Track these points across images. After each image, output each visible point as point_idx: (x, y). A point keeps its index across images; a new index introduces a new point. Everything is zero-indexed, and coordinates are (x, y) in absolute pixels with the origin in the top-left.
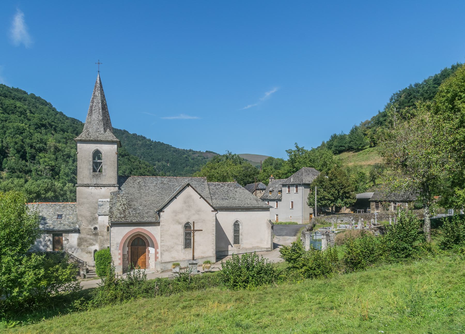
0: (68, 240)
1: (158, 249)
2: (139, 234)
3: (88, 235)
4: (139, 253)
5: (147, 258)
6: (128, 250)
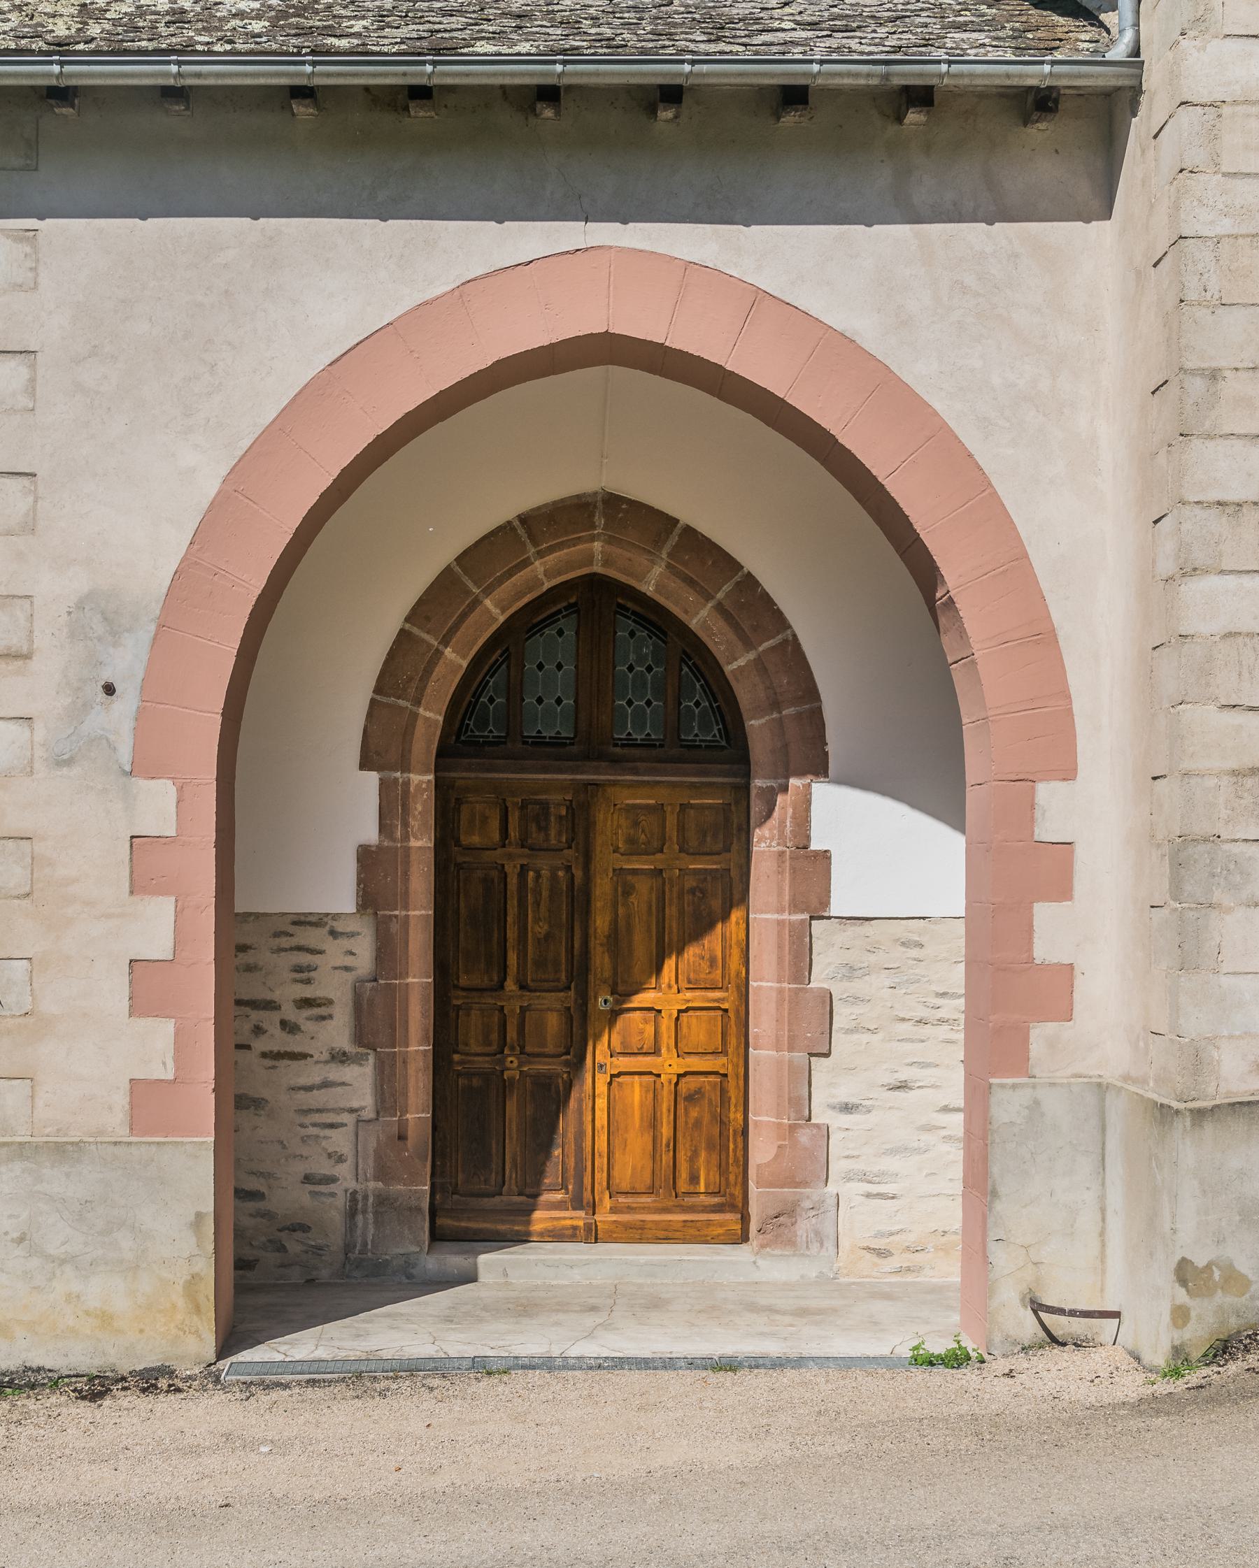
1: (1068, 773)
2: (613, 502)
4: (601, 922)
5: (763, 1024)
6: (370, 833)
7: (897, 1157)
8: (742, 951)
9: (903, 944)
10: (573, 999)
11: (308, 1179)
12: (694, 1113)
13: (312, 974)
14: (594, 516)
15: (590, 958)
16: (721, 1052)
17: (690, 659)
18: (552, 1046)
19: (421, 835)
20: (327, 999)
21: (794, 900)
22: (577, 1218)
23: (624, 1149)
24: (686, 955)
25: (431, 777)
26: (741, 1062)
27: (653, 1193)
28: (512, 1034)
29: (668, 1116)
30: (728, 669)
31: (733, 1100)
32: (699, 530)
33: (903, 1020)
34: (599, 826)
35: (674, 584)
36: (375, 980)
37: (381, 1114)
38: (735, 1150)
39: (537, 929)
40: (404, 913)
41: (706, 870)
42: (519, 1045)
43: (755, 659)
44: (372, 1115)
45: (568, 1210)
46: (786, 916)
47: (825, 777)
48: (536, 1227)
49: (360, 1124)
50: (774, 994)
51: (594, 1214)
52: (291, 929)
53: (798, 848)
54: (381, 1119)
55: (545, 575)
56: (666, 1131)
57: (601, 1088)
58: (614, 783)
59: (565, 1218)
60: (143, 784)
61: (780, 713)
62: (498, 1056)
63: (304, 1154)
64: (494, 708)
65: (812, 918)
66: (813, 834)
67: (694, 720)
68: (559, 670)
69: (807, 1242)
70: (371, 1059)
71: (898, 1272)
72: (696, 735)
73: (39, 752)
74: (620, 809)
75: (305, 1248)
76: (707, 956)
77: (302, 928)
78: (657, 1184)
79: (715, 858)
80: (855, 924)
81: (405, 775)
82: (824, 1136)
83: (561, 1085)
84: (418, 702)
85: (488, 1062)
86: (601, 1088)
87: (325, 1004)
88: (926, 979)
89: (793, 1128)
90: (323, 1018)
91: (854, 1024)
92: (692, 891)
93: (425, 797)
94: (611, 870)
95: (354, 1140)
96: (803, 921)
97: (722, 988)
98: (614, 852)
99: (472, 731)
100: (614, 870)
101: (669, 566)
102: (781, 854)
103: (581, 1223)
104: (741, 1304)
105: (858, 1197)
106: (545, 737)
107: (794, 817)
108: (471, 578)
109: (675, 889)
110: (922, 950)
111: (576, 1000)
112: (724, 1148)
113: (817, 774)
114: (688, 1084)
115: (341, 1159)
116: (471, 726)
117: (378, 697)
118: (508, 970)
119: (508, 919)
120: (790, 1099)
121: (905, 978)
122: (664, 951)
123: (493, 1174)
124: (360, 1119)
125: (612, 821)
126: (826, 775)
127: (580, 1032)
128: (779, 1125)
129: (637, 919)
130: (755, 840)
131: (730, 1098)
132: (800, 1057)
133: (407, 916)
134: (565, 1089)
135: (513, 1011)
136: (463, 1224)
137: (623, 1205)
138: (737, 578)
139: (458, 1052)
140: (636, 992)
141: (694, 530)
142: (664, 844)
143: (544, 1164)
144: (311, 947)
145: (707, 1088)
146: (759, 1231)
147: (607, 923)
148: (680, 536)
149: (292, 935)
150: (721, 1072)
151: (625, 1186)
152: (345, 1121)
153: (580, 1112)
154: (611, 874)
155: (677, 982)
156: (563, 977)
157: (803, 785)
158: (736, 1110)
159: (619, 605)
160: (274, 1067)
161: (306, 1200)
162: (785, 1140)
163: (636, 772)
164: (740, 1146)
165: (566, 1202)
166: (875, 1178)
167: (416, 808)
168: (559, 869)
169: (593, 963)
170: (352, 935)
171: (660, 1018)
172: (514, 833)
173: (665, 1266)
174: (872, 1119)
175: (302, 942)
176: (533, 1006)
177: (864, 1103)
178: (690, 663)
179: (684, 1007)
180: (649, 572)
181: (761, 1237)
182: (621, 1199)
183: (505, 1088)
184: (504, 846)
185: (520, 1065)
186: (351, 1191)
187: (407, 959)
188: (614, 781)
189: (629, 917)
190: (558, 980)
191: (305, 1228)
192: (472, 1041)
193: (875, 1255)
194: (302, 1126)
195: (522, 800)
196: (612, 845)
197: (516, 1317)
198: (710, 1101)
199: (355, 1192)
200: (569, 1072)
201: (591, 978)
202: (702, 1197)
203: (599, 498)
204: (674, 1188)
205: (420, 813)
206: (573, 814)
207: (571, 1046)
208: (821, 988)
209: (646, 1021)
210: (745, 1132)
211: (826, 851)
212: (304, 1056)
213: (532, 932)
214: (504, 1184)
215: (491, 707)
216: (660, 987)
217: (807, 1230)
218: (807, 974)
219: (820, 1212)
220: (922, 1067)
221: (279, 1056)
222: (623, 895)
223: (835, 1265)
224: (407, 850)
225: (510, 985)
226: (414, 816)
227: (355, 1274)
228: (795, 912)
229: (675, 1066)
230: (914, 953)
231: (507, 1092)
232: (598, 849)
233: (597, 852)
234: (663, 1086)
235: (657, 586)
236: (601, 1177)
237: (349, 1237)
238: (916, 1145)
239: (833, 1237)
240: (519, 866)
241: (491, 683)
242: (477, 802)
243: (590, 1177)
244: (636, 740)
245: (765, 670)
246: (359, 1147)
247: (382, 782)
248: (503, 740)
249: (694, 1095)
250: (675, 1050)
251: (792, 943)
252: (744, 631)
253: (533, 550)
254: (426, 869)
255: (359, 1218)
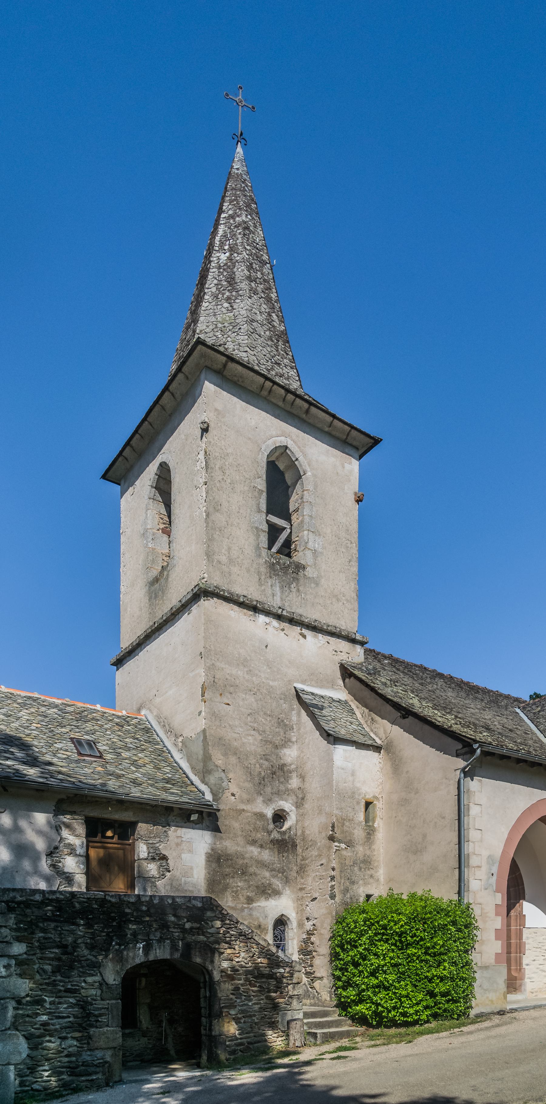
0: (164, 858)
3: (254, 842)
60: (497, 894)
73: (483, 887)
230: (536, 934)
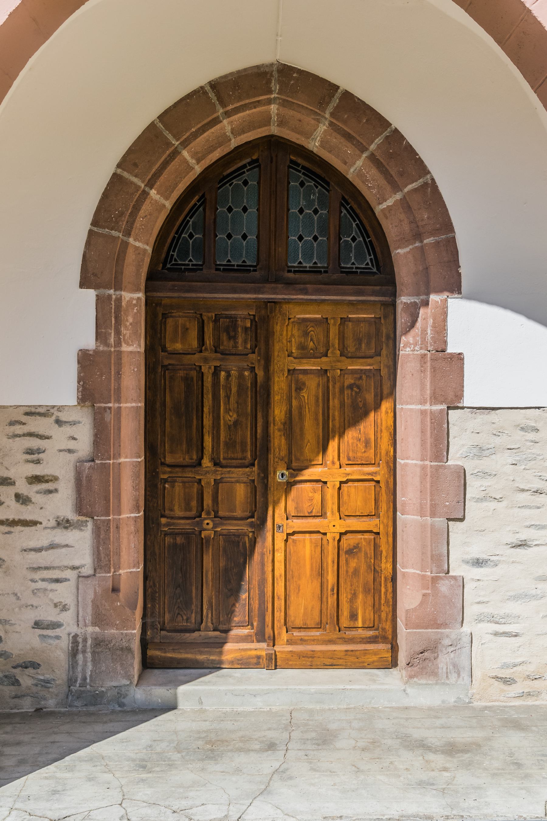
7: (519, 602)
8: (390, 434)
9: (522, 429)
10: (256, 472)
11: (37, 625)
12: (353, 564)
13: (41, 456)
14: (271, 83)
15: (270, 441)
16: (374, 515)
17: (348, 204)
18: (240, 512)
19: (132, 341)
20: (53, 476)
21: (434, 393)
22: (260, 649)
23: (298, 593)
24: (346, 437)
25: (141, 295)
26: (391, 523)
27: (321, 628)
28: (208, 501)
29: (333, 567)
30: (378, 209)
31: (384, 553)
32: (355, 95)
33: (523, 490)
34: (277, 334)
35: (336, 140)
36: (93, 460)
37: (98, 571)
38: (386, 593)
39: (228, 417)
40: (117, 405)
41: (362, 370)
42: (213, 511)
43: (401, 199)
44: (91, 572)
45: (253, 642)
46: (427, 407)
47: (458, 293)
48: (227, 657)
49: (80, 579)
50: (418, 470)
51: (274, 646)
52: (24, 419)
53: (437, 351)
54: (98, 575)
55: (232, 133)
56: (331, 578)
57: (280, 544)
58: (288, 302)
59: (251, 650)
61: (421, 242)
62: (197, 519)
63: (35, 604)
64: (192, 242)
65: (449, 408)
66: (449, 340)
67: (351, 251)
68: (245, 213)
69: (447, 673)
70: (90, 525)
71: (521, 696)
72: (353, 264)
74: (294, 322)
75: (35, 682)
76: (363, 439)
77: (33, 417)
78: (324, 621)
79: (369, 361)
80: (484, 413)
81: (118, 293)
82: (460, 586)
83: (247, 542)
84: (128, 233)
85: (188, 524)
86: (280, 544)
87: (51, 481)
88: (541, 457)
89: (435, 580)
90: (50, 492)
91: (483, 494)
92: (351, 387)
93: (135, 311)
94: (286, 370)
95: (76, 593)
96: (441, 411)
97: (374, 464)
98: (289, 356)
99: (176, 260)
100: (289, 371)
101: (331, 124)
102: (424, 356)
103: (263, 653)
104: (397, 738)
105: (487, 635)
106: (234, 265)
107: (434, 326)
108: (171, 132)
109: (338, 385)
110: (538, 434)
111: (259, 474)
112: (377, 591)
113: (452, 291)
114: (349, 541)
115: (65, 608)
116: (175, 256)
117: (95, 229)
118: (205, 450)
119: (205, 409)
120: (432, 556)
121: (525, 456)
122: (329, 435)
123: (193, 615)
124: (81, 575)
125: (287, 331)
126: (460, 292)
127: (262, 499)
128: (423, 577)
129: (307, 410)
130: (402, 345)
131: (382, 552)
132: (440, 521)
133: (120, 408)
134: (250, 545)
135: (208, 483)
136: (169, 655)
137: (297, 638)
138: (386, 133)
139: (163, 516)
140: (306, 468)
141: (352, 94)
142: (328, 350)
143: (234, 605)
144: (40, 433)
145: (364, 543)
146: (408, 664)
147: (283, 413)
148: (341, 99)
149: (24, 424)
150: (375, 531)
151: (299, 622)
152: (68, 577)
153: (263, 564)
154: (286, 374)
155: (339, 459)
156: (249, 455)
157: (441, 300)
158: (387, 562)
159: (292, 161)
160: (9, 533)
161: (36, 642)
162: (428, 589)
163: (305, 292)
164: (390, 590)
165: (251, 636)
166: (501, 620)
167: (127, 320)
168: (244, 369)
169: (272, 445)
170: (74, 423)
171: (326, 487)
172: (209, 341)
173: (332, 694)
174: (498, 571)
175: (33, 429)
176: (225, 479)
177: (492, 558)
178: (348, 207)
179: (344, 479)
180: (315, 130)
181: (409, 669)
182: (296, 633)
183: (203, 544)
184: (201, 351)
185: (215, 526)
186: (73, 634)
187: (120, 442)
188: (288, 299)
189: (300, 408)
190: (244, 458)
191: (35, 665)
192: (176, 508)
193: (502, 683)
194: (33, 581)
195: (216, 315)
196: (287, 350)
197: (202, 760)
198: (366, 554)
199: (76, 636)
200: (253, 532)
201: (271, 456)
202: (360, 631)
203: (275, 68)
204: (338, 624)
205: (131, 324)
206: (256, 326)
207: (255, 511)
208: (457, 465)
209: (314, 491)
210: (394, 579)
211: (460, 354)
212: (34, 523)
213: (224, 420)
214: (202, 622)
215: (191, 242)
216: (326, 463)
217: (447, 663)
218: (445, 453)
219: (457, 648)
220: (539, 529)
221: (13, 523)
222: (296, 390)
223: (470, 692)
224: (119, 354)
225: (206, 462)
226: (126, 327)
227: (76, 703)
228: (435, 404)
229: (337, 526)
230: (531, 436)
231: (204, 549)
232: (276, 354)
233: (276, 357)
234: (328, 543)
235: (322, 141)
236: (279, 615)
237: (71, 673)
238: (534, 592)
239: (468, 669)
240: (213, 367)
241: (191, 223)
242: (179, 317)
243: (271, 616)
244: (306, 267)
245: (409, 207)
246: (80, 598)
247: (99, 298)
248: (201, 267)
249: (353, 550)
250: (337, 514)
251: (433, 429)
252: (392, 176)
253: (221, 111)
254: (136, 370)
255: (80, 657)
